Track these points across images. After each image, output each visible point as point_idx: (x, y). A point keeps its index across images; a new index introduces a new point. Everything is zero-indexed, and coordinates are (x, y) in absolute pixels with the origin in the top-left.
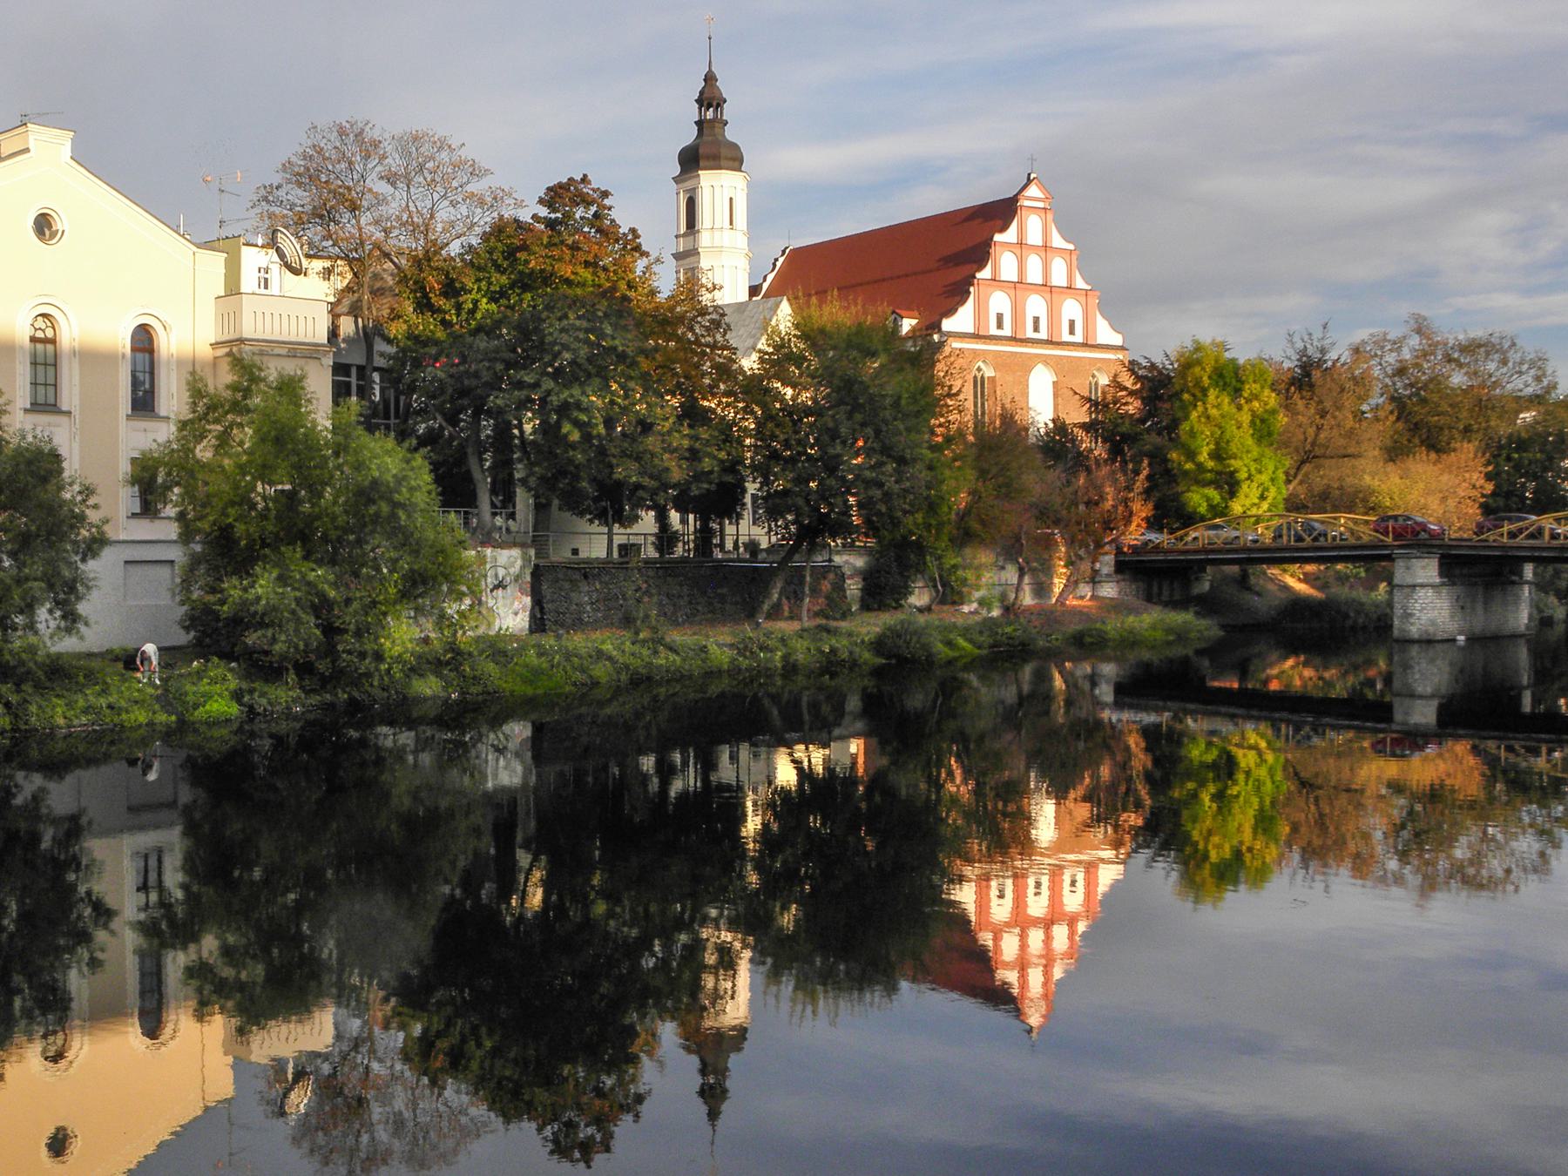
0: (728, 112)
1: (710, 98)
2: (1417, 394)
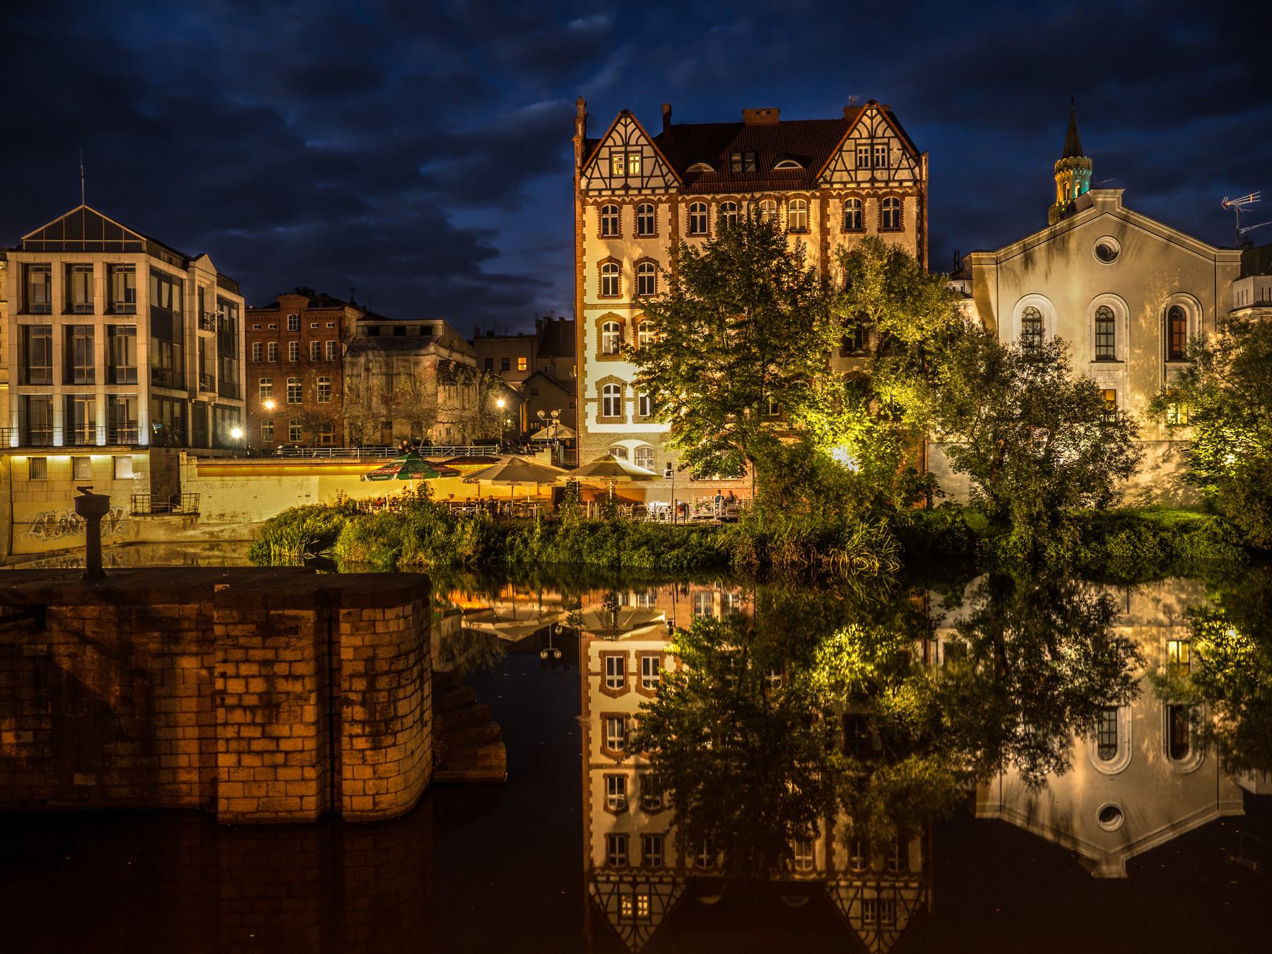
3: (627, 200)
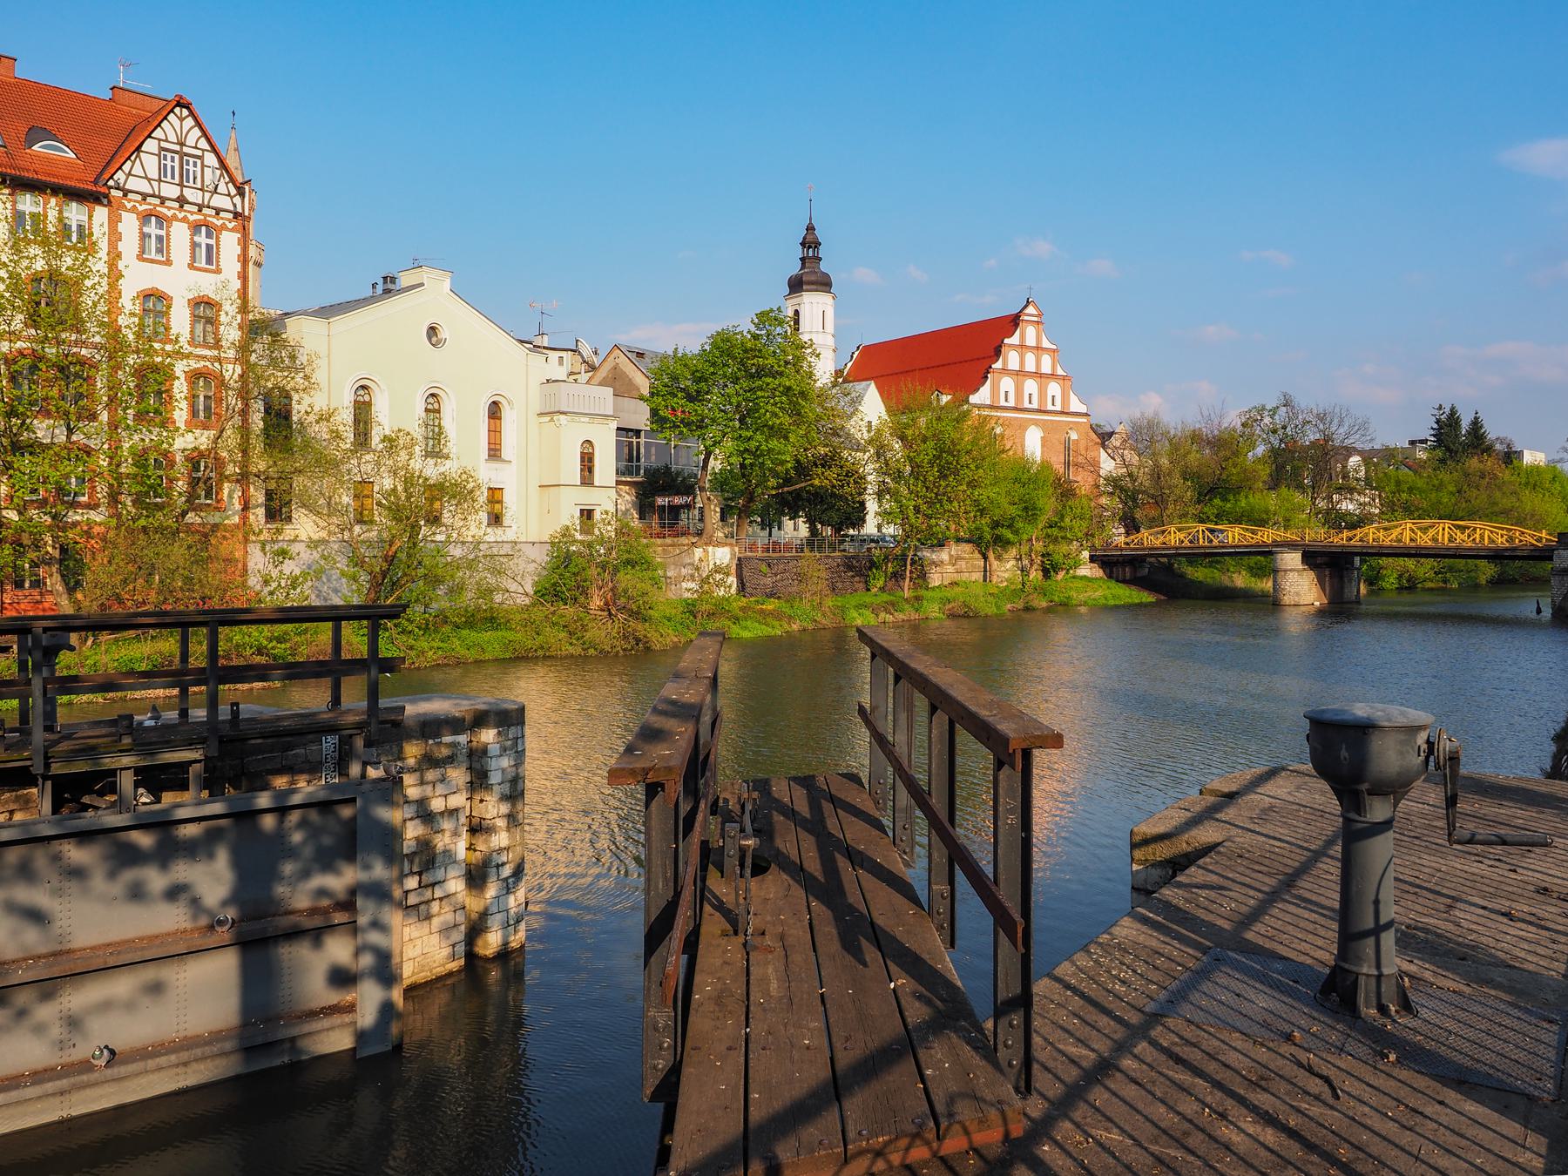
0: (822, 252)
1: (810, 242)
2: (590, 545)
3: (180, 216)
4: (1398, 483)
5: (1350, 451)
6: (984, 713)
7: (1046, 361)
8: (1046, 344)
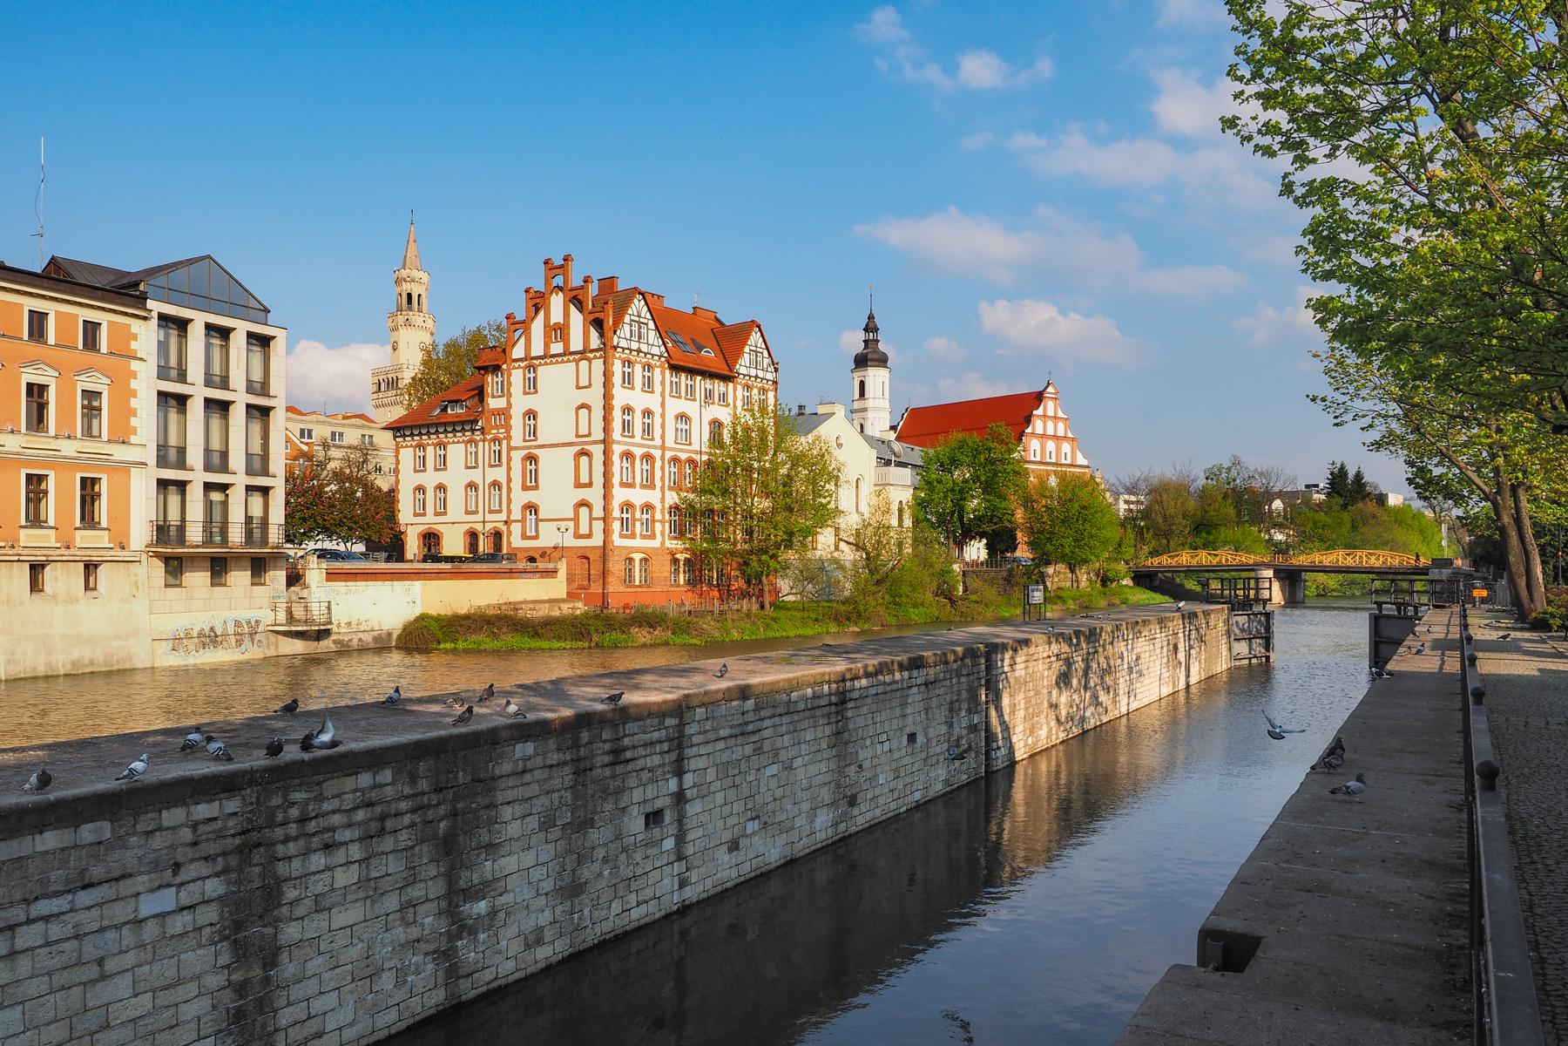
4: (1315, 523)
5: (1269, 496)
6: (74, 737)
7: (1061, 426)
8: (1060, 414)
